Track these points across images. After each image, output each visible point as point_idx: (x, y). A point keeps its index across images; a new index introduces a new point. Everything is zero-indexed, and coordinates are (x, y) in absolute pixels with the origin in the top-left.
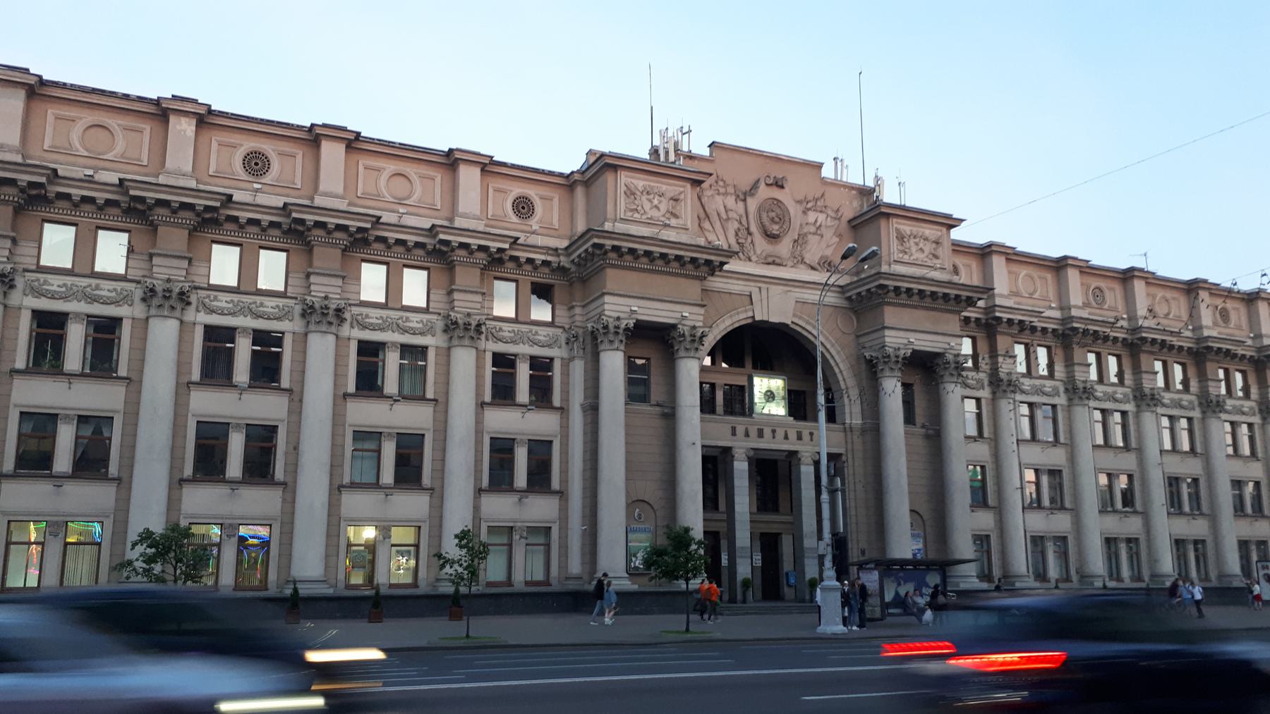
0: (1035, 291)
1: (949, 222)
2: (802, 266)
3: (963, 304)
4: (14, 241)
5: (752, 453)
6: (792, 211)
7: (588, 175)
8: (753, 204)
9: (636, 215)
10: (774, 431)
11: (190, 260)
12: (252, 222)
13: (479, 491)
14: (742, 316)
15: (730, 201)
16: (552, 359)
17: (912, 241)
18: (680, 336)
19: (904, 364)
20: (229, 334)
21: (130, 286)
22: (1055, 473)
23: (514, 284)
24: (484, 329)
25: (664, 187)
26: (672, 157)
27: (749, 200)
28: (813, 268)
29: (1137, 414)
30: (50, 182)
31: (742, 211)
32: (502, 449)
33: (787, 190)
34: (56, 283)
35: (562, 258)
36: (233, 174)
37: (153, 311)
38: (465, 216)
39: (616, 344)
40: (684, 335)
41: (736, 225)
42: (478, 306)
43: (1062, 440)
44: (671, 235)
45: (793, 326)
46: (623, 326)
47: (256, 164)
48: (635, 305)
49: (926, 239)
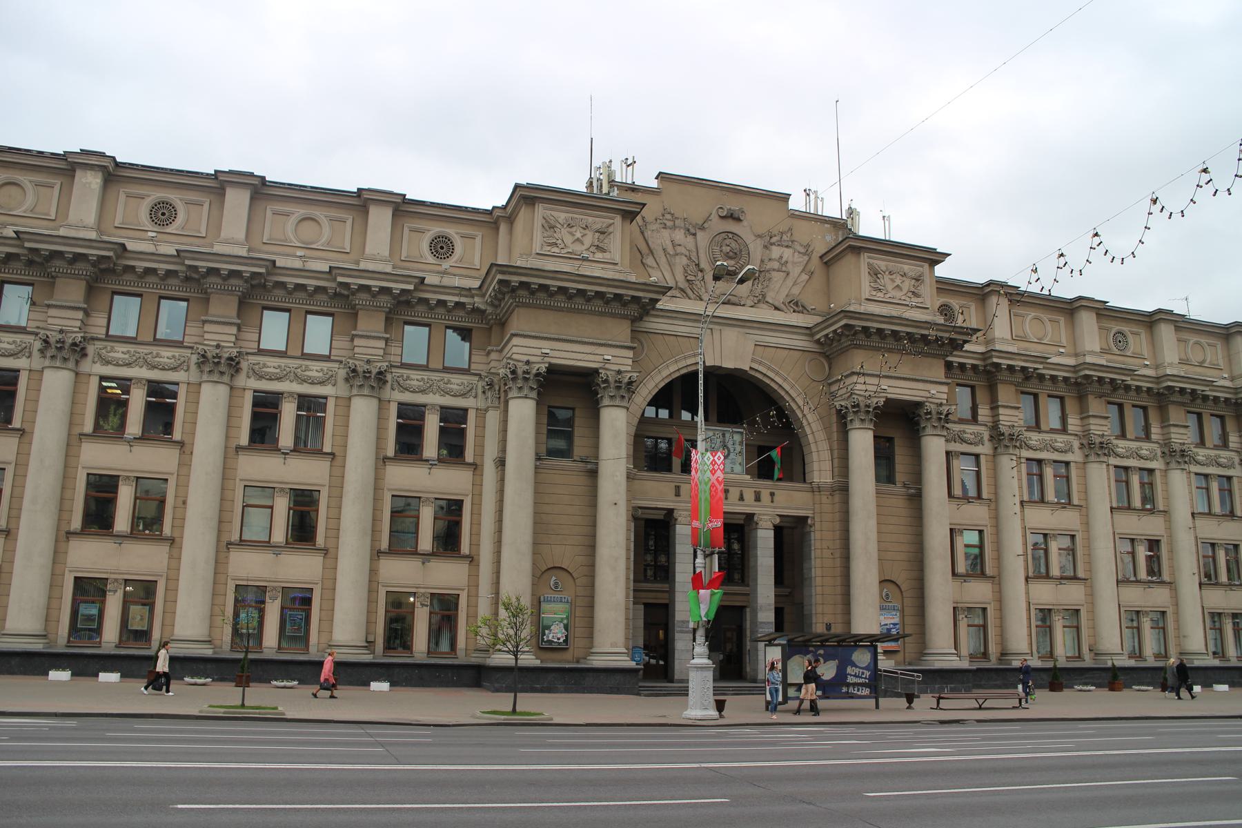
1: (933, 257)
2: (765, 306)
3: (948, 348)
4: (87, 313)
5: (778, 520)
6: (751, 247)
7: (509, 209)
9: (556, 250)
11: (387, 340)
12: (149, 271)
13: (377, 554)
15: (679, 236)
16: (466, 410)
17: (887, 277)
18: (927, 413)
19: (541, 385)
20: (125, 384)
21: (30, 338)
22: (1154, 544)
25: (590, 219)
27: (700, 234)
28: (776, 308)
29: (995, 454)
30: (118, 257)
31: (691, 246)
32: (404, 509)
33: (745, 223)
36: (286, 240)
37: (355, 391)
38: (373, 259)
39: (526, 391)
40: (606, 381)
41: (685, 261)
43: (985, 495)
44: (596, 271)
45: (753, 373)
46: (534, 371)
47: (163, 214)
48: (546, 346)
49: (904, 275)
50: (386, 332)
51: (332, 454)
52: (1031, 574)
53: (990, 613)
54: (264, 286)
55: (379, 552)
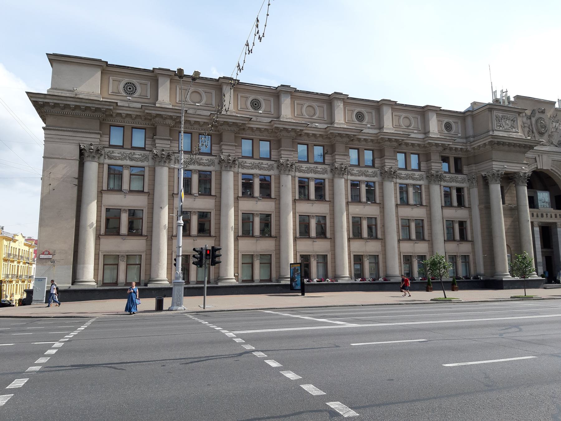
0: (315, 114)
5: (540, 224)
8: (533, 120)
10: (547, 215)
14: (533, 167)
23: (357, 150)
24: (237, 162)
26: (506, 103)
31: (529, 123)
34: (305, 167)
35: (468, 147)
36: (119, 93)
42: (169, 146)
47: (130, 89)
50: (235, 142)
51: (215, 196)
52: (401, 238)
53: (143, 257)
54: (112, 115)
55: (238, 236)
